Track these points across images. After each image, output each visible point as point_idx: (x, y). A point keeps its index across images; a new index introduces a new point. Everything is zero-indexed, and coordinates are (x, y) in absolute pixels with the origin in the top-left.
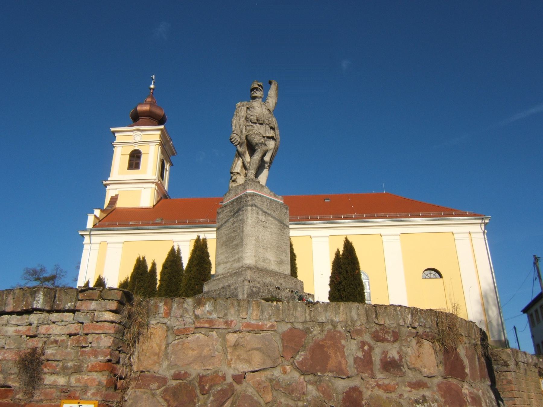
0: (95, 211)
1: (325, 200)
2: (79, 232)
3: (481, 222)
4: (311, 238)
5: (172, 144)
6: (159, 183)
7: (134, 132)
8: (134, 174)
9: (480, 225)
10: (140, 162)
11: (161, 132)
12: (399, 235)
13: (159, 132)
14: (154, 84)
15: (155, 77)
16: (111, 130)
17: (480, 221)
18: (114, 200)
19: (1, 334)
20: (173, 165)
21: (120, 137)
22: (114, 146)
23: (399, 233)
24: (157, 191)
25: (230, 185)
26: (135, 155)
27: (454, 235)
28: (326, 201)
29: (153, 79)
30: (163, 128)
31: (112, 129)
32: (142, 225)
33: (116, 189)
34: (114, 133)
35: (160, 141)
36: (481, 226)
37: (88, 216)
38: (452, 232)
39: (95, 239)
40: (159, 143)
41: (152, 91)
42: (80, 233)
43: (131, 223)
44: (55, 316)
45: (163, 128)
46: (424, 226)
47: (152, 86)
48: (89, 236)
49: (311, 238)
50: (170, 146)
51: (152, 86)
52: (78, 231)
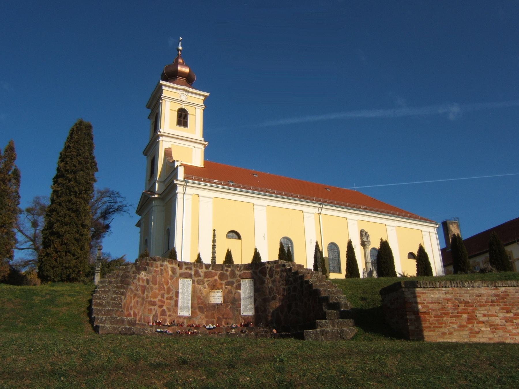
1: (254, 175)
3: (319, 206)
4: (198, 196)
7: (181, 91)
9: (183, 186)
12: (192, 195)
13: (203, 98)
16: (161, 83)
17: (319, 206)
19: (518, 306)
23: (213, 196)
27: (200, 197)
28: (255, 176)
30: (208, 95)
32: (277, 194)
36: (183, 187)
38: (302, 211)
39: (189, 190)
40: (203, 108)
41: (180, 52)
43: (215, 181)
44: (463, 288)
46: (210, 191)
47: (180, 48)
48: (183, 186)
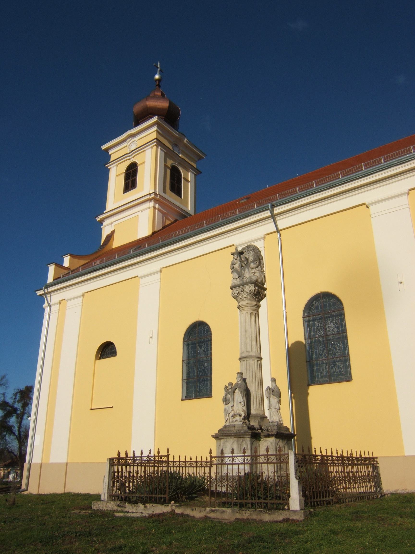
0: (65, 258)
2: (37, 292)
4: (368, 207)
5: (187, 141)
6: (158, 198)
7: (128, 140)
8: (133, 195)
10: (137, 177)
11: (157, 127)
13: (155, 128)
14: (159, 73)
15: (161, 65)
18: (110, 237)
20: (201, 173)
21: (114, 154)
22: (109, 168)
24: (159, 210)
25: (314, 181)
26: (131, 171)
29: (158, 68)
30: (157, 119)
31: (104, 147)
33: (112, 223)
34: (107, 150)
35: (156, 140)
37: (48, 268)
40: (155, 144)
42: (38, 294)
45: (157, 119)
49: (368, 207)
50: (185, 145)
51: (157, 77)
52: (36, 291)
